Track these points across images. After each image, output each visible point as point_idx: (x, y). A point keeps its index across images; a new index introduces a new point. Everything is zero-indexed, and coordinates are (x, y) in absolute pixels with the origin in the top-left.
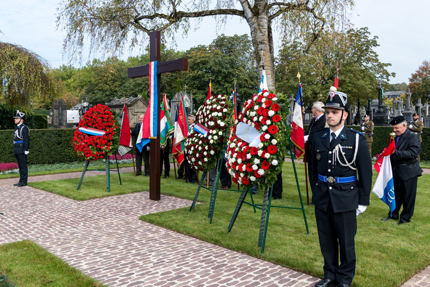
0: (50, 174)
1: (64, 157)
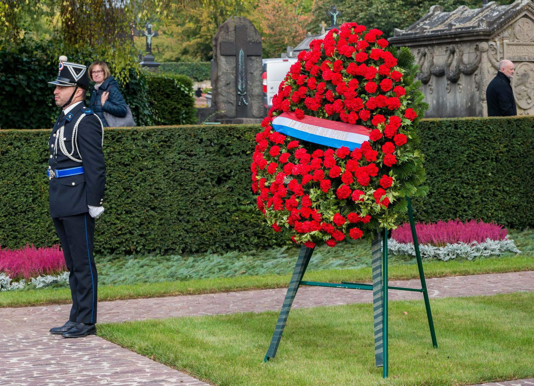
0: (182, 293)
1: (238, 231)
